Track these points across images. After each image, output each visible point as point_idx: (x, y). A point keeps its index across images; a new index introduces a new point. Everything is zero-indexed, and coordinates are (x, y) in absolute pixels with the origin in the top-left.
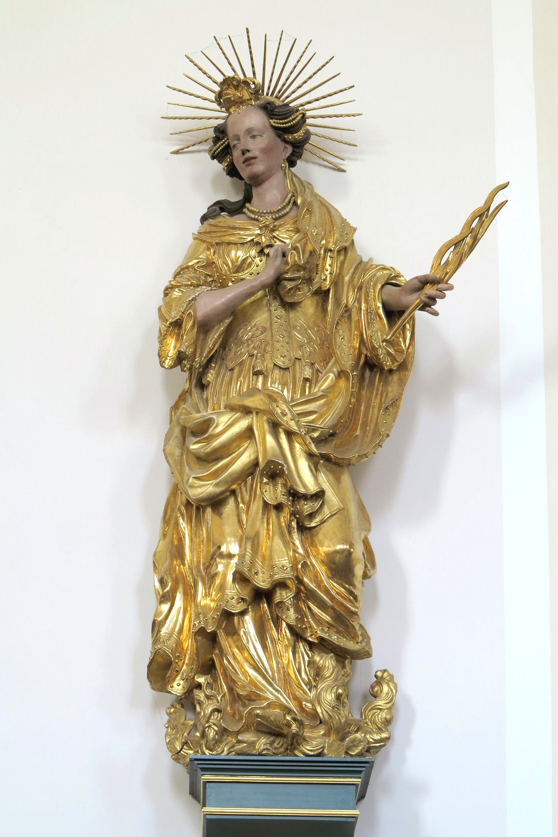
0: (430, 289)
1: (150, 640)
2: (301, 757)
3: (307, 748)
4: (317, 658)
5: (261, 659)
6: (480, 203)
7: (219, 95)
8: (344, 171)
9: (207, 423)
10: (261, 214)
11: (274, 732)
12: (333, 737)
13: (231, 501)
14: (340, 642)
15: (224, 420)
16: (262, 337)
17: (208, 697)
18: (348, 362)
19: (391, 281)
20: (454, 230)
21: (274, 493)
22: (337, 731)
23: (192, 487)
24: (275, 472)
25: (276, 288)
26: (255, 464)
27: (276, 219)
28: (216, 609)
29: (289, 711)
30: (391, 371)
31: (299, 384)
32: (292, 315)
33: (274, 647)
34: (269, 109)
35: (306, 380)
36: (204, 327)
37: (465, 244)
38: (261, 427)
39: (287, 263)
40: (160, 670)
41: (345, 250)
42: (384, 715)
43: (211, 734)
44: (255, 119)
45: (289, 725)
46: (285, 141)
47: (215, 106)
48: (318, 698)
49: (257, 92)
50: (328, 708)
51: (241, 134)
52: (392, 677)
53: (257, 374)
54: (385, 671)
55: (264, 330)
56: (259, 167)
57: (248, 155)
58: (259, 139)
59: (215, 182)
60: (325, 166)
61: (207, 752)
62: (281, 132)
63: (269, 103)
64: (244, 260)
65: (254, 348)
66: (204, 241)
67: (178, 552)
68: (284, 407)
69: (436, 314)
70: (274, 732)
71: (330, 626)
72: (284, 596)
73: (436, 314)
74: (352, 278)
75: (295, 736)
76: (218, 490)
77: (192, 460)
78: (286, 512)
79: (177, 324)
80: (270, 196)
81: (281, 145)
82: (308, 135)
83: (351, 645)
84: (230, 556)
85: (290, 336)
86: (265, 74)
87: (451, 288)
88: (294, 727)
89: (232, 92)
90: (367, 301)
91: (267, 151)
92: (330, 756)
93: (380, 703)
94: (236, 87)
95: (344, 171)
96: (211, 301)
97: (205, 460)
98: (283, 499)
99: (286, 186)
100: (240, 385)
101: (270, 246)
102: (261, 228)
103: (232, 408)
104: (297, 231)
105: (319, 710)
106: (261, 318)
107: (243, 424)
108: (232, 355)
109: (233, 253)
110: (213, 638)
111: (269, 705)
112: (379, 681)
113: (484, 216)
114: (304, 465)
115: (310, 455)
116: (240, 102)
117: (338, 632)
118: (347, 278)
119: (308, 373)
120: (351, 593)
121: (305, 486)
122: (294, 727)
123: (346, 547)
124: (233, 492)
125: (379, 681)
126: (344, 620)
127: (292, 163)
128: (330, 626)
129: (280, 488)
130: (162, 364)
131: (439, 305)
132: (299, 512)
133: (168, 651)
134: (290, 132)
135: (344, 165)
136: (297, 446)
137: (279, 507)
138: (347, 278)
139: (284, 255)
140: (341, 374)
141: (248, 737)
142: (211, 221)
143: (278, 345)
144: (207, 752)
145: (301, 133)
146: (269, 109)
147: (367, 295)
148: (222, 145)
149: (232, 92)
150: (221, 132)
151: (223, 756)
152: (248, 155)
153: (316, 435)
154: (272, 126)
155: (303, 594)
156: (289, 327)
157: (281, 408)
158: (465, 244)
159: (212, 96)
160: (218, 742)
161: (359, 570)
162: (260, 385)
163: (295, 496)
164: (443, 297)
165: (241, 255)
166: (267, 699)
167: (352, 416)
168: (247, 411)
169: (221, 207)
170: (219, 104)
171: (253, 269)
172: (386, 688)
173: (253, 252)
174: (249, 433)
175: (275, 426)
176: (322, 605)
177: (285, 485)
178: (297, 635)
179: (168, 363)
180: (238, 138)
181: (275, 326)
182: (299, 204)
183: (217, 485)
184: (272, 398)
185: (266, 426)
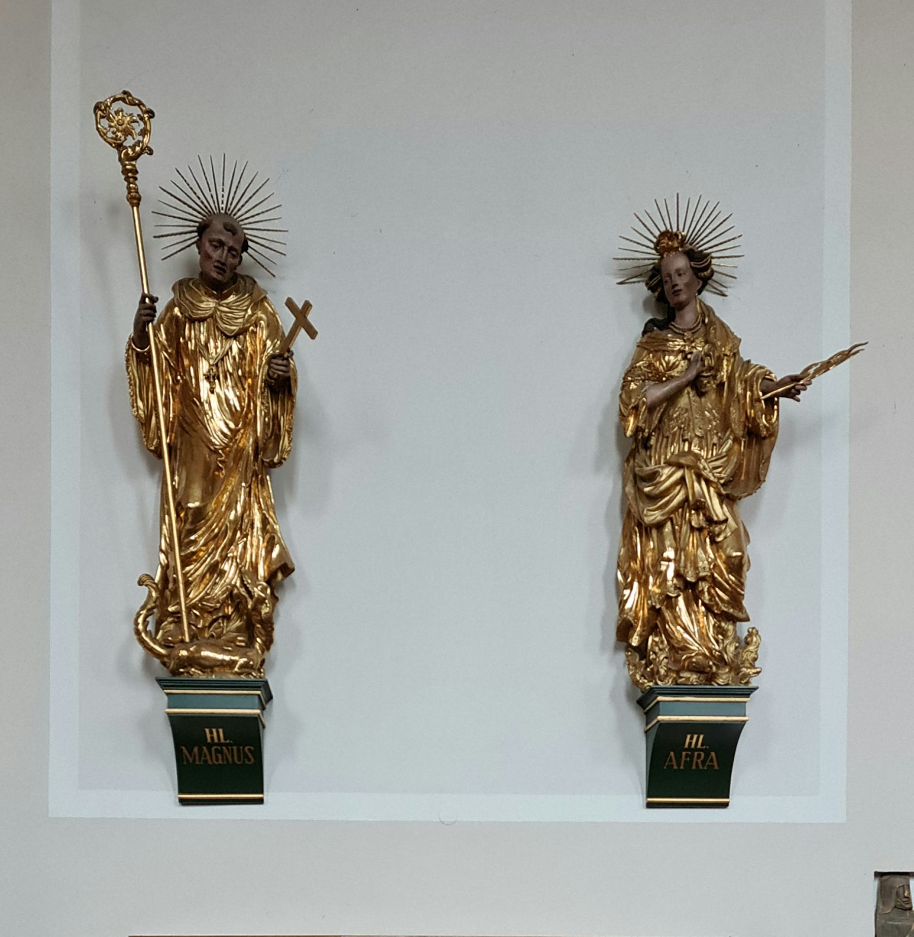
0: (794, 387)
1: (616, 611)
2: (716, 686)
3: (720, 681)
4: (723, 624)
5: (691, 625)
7: (657, 244)
8: (725, 296)
9: (654, 475)
10: (684, 331)
11: (698, 669)
12: (733, 674)
13: (669, 524)
14: (729, 612)
15: (667, 471)
16: (686, 415)
17: (660, 650)
18: (740, 432)
19: (766, 377)
21: (697, 520)
22: (736, 670)
23: (646, 516)
24: (700, 506)
25: (696, 385)
26: (686, 499)
27: (693, 333)
28: (660, 594)
29: (704, 655)
30: (765, 438)
32: (703, 400)
33: (696, 616)
35: (714, 444)
36: (651, 409)
38: (690, 477)
39: (704, 366)
40: (624, 630)
41: (734, 354)
42: (753, 655)
43: (662, 672)
44: (681, 262)
45: (711, 667)
46: (698, 277)
47: (654, 252)
48: (725, 649)
49: (683, 242)
50: (731, 655)
51: (672, 272)
52: (757, 631)
54: (753, 628)
55: (687, 411)
56: (683, 297)
57: (677, 288)
58: (683, 277)
60: (715, 293)
61: (659, 683)
62: (696, 271)
63: (692, 250)
64: (674, 363)
65: (682, 423)
66: (645, 349)
67: (632, 556)
68: (705, 464)
69: (798, 400)
70: (698, 669)
72: (704, 586)
73: (798, 400)
74: (740, 375)
75: (714, 674)
76: (663, 518)
77: (644, 497)
78: (706, 532)
79: (636, 408)
80: (688, 317)
81: (696, 280)
83: (740, 615)
84: (669, 560)
85: (703, 414)
88: (714, 669)
90: (751, 391)
91: (687, 285)
93: (751, 648)
94: (670, 239)
95: (725, 296)
96: (656, 392)
97: (652, 498)
99: (696, 310)
100: (674, 449)
101: (691, 353)
102: (684, 341)
103: (669, 464)
104: (706, 342)
105: (726, 657)
106: (683, 401)
107: (678, 474)
108: (666, 427)
109: (667, 358)
111: (696, 655)
112: (750, 634)
114: (716, 501)
115: (719, 495)
116: (670, 249)
117: (733, 607)
118: (737, 375)
119: (715, 440)
120: (740, 581)
121: (717, 516)
122: (714, 669)
123: (739, 554)
126: (736, 599)
127: (700, 292)
128: (728, 603)
129: (701, 517)
131: (802, 395)
132: (713, 532)
133: (631, 619)
134: (702, 270)
135: (727, 292)
136: (712, 489)
137: (700, 529)
138: (737, 375)
139: (702, 360)
140: (736, 440)
142: (649, 334)
143: (696, 421)
144: (659, 683)
145: (709, 271)
147: (752, 387)
148: (655, 278)
149: (667, 242)
151: (668, 686)
152: (677, 288)
153: (722, 481)
154: (691, 267)
155: (715, 583)
156: (702, 410)
157: (702, 464)
162: (686, 449)
163: (710, 521)
164: (805, 390)
165: (672, 359)
166: (694, 651)
168: (680, 466)
171: (680, 367)
172: (755, 639)
173: (680, 357)
174: (682, 481)
175: (699, 476)
176: (724, 590)
177: (704, 515)
178: (709, 609)
180: (670, 276)
181: (694, 408)
182: (708, 324)
183: (663, 515)
184: (698, 457)
185: (694, 477)
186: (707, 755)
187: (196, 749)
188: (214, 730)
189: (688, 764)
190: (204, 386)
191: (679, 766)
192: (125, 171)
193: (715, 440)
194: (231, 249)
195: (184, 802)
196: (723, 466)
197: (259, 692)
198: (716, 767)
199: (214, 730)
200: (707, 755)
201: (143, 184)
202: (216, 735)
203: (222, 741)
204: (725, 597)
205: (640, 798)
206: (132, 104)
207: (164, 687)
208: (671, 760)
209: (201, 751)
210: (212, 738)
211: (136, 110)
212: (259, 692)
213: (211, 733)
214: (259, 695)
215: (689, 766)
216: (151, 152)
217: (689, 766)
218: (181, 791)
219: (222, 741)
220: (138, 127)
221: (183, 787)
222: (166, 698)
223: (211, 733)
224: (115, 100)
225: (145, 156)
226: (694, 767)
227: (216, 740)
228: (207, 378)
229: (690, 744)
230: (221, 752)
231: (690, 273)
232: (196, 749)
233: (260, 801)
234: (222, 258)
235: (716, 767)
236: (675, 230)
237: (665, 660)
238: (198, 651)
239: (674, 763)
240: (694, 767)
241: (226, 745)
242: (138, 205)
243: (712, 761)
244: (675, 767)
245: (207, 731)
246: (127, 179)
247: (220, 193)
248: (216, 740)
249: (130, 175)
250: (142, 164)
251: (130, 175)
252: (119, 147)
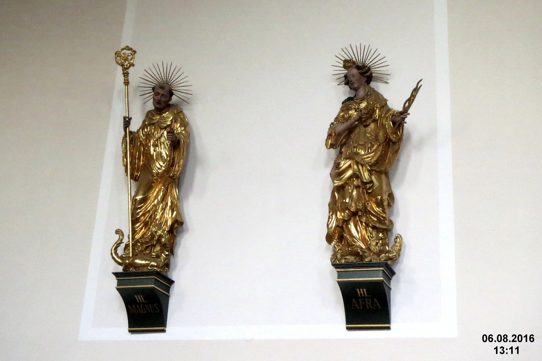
6: (415, 86)
11: (356, 254)
20: (408, 96)
31: (367, 149)
34: (358, 68)
35: (369, 148)
36: (339, 135)
37: (410, 101)
44: (355, 71)
46: (364, 76)
47: (343, 69)
53: (354, 147)
59: (350, 92)
62: (362, 74)
70: (356, 254)
71: (376, 221)
75: (362, 256)
80: (361, 93)
82: (371, 73)
86: (358, 58)
87: (409, 114)
89: (348, 64)
92: (374, 261)
93: (397, 244)
98: (360, 184)
110: (342, 227)
112: (397, 238)
113: (416, 90)
124: (347, 184)
125: (397, 238)
130: (327, 147)
135: (388, 81)
141: (348, 257)
146: (358, 68)
148: (347, 81)
149: (348, 64)
150: (346, 76)
158: (410, 101)
159: (342, 66)
160: (341, 259)
161: (385, 203)
167: (369, 157)
169: (349, 99)
170: (345, 68)
172: (398, 240)
176: (373, 215)
178: (367, 225)
179: (329, 147)
186: (373, 301)
187: (134, 306)
188: (361, 290)
189: (364, 306)
190: (152, 149)
191: (359, 306)
192: (124, 74)
193: (370, 145)
194: (163, 95)
195: (348, 329)
196: (373, 157)
197: (382, 269)
198: (380, 307)
199: (361, 290)
200: (373, 301)
201: (131, 78)
202: (362, 292)
203: (366, 295)
204: (375, 219)
205: (344, 325)
206: (128, 50)
207: (336, 268)
208: (354, 304)
209: (136, 306)
210: (361, 294)
211: (130, 52)
212: (382, 269)
213: (360, 291)
214: (383, 270)
215: (367, 305)
216: (133, 65)
217: (367, 305)
218: (347, 323)
219: (366, 295)
220: (130, 58)
221: (348, 322)
222: (336, 273)
223: (360, 291)
224: (122, 49)
225: (132, 68)
226: (368, 308)
227: (363, 296)
228: (153, 145)
229: (361, 294)
230: (145, 307)
231: (359, 75)
232: (134, 306)
233: (389, 328)
234: (165, 98)
235: (380, 307)
236: (354, 59)
237: (340, 251)
238: (134, 260)
239: (357, 305)
240: (368, 308)
241: (367, 298)
242: (128, 85)
243: (376, 304)
244: (358, 308)
245: (358, 290)
246: (124, 76)
247: (163, 75)
248: (363, 296)
249: (126, 74)
250: (131, 70)
251: (126, 74)
252: (122, 65)
